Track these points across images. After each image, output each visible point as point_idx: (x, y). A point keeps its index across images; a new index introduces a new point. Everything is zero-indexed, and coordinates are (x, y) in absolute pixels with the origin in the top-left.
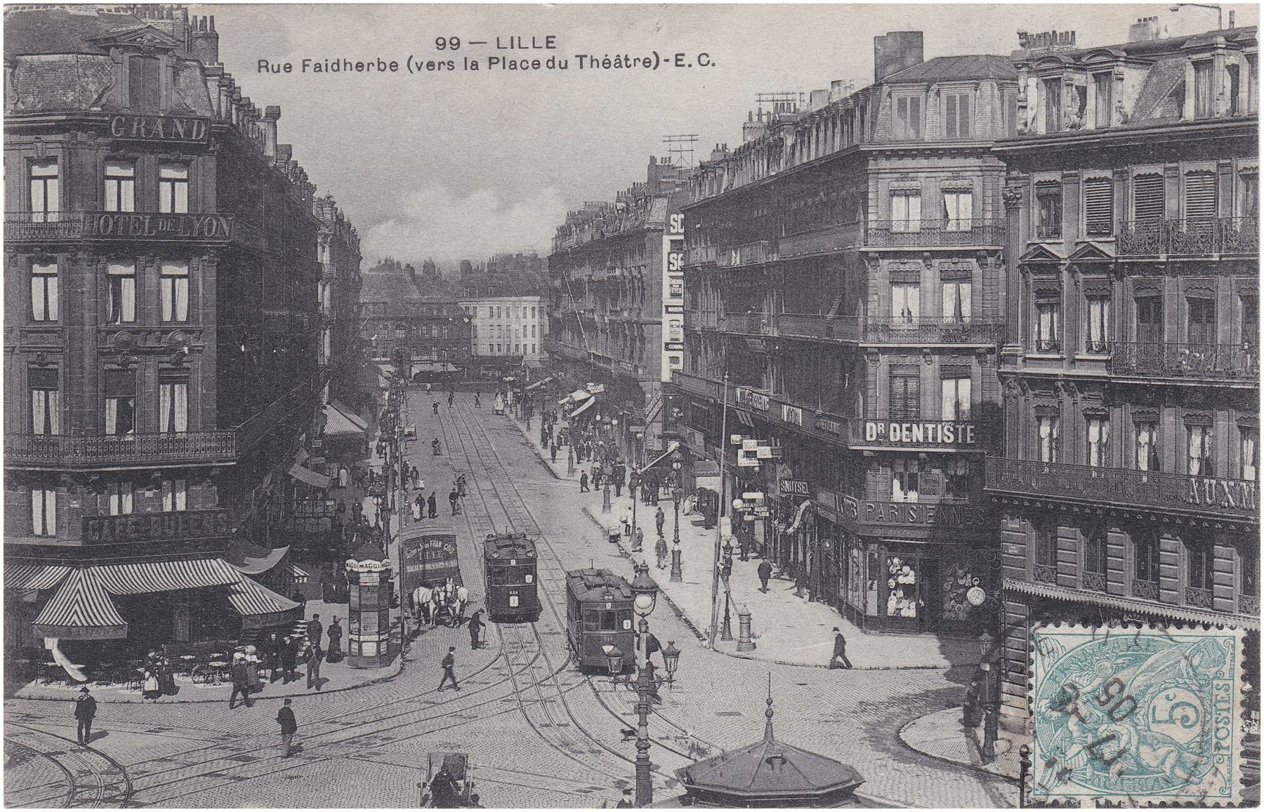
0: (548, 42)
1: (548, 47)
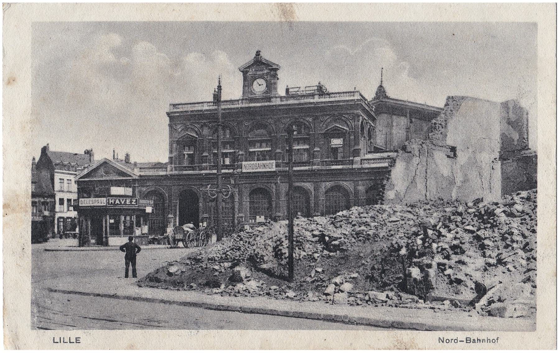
0: (76, 340)
1: (76, 342)
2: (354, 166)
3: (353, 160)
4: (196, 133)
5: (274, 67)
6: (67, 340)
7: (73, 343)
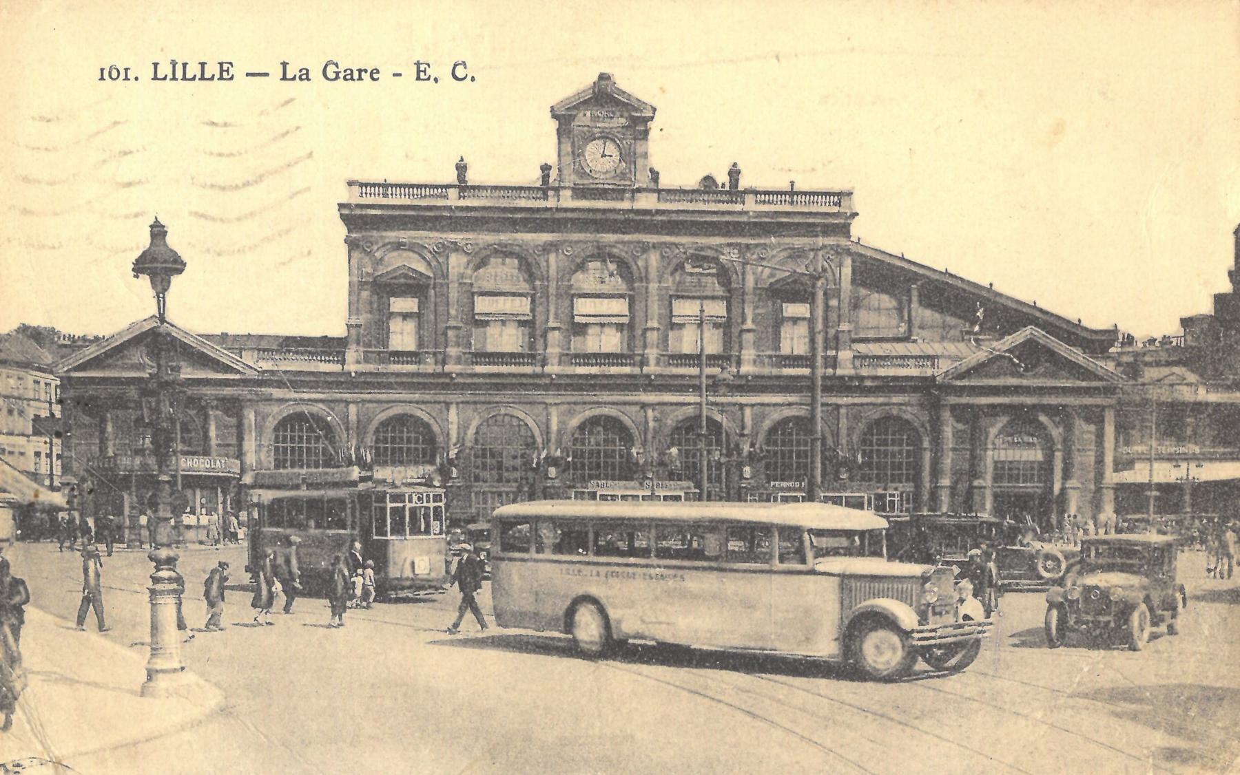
1: (221, 78)
2: (839, 372)
3: (835, 358)
4: (429, 264)
5: (648, 114)
6: (193, 70)
7: (294, 79)
